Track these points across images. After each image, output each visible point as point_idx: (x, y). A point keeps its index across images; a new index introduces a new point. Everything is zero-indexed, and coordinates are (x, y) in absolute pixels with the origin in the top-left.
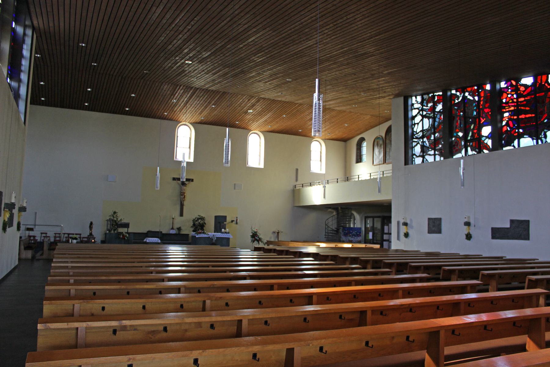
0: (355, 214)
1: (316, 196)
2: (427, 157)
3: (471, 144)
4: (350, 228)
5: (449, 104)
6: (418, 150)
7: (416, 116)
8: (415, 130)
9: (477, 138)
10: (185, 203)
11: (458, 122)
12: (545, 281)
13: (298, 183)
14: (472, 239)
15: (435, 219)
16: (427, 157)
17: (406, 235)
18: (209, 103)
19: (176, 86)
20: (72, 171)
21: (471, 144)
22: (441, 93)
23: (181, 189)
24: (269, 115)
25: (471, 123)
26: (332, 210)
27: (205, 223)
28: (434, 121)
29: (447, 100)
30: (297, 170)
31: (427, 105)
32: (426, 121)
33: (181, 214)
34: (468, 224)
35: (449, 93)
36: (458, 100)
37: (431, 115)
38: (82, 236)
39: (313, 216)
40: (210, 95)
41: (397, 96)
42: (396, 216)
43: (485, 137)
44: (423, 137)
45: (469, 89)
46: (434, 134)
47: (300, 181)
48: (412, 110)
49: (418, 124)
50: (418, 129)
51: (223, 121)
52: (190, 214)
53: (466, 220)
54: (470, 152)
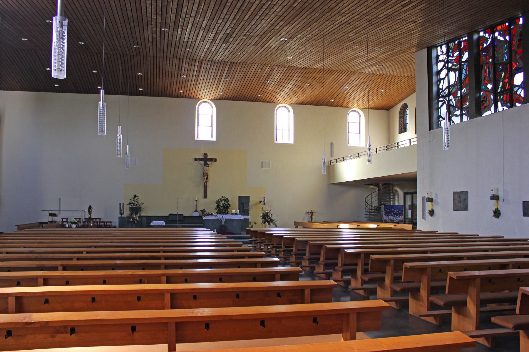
0: (398, 189)
1: (351, 171)
2: (454, 118)
3: (501, 97)
4: (394, 207)
5: (475, 51)
6: (444, 110)
7: (442, 70)
8: (441, 87)
9: (508, 89)
10: (209, 184)
11: (487, 72)
12: (478, 281)
13: (333, 158)
14: (500, 217)
15: (460, 192)
16: (454, 118)
17: (432, 213)
18: (221, 76)
19: (180, 60)
20: (86, 155)
21: (501, 97)
22: (466, 38)
23: (203, 169)
24: (291, 85)
25: (502, 71)
26: (375, 187)
27: (230, 205)
28: (461, 74)
29: (474, 46)
30: (332, 144)
31: (453, 54)
32: (452, 74)
33: (205, 196)
34: (495, 198)
35: (475, 37)
36: (486, 43)
37: (457, 67)
38: (101, 220)
39: (352, 193)
40: (307, 74)
41: (419, 47)
42: (421, 192)
43: (518, 86)
44: (449, 95)
45: (499, 28)
46: (461, 89)
47: (335, 157)
48: (437, 63)
49: (444, 79)
50: (444, 85)
51: (246, 95)
52: (214, 195)
53: (493, 193)
54: (500, 108)
